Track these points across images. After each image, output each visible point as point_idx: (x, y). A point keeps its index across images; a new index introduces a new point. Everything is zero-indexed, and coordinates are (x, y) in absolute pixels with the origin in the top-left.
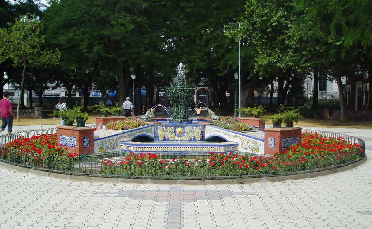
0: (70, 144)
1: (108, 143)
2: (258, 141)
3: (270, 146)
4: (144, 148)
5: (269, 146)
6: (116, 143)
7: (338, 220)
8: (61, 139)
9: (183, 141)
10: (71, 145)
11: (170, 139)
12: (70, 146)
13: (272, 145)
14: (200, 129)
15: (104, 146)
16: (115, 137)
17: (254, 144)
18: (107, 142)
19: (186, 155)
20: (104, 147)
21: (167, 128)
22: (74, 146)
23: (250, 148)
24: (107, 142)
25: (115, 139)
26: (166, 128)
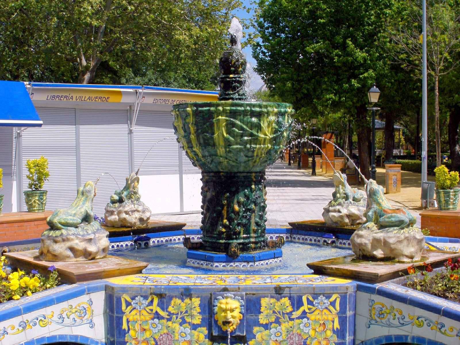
14: (333, 304)
21: (168, 304)
26: (163, 306)
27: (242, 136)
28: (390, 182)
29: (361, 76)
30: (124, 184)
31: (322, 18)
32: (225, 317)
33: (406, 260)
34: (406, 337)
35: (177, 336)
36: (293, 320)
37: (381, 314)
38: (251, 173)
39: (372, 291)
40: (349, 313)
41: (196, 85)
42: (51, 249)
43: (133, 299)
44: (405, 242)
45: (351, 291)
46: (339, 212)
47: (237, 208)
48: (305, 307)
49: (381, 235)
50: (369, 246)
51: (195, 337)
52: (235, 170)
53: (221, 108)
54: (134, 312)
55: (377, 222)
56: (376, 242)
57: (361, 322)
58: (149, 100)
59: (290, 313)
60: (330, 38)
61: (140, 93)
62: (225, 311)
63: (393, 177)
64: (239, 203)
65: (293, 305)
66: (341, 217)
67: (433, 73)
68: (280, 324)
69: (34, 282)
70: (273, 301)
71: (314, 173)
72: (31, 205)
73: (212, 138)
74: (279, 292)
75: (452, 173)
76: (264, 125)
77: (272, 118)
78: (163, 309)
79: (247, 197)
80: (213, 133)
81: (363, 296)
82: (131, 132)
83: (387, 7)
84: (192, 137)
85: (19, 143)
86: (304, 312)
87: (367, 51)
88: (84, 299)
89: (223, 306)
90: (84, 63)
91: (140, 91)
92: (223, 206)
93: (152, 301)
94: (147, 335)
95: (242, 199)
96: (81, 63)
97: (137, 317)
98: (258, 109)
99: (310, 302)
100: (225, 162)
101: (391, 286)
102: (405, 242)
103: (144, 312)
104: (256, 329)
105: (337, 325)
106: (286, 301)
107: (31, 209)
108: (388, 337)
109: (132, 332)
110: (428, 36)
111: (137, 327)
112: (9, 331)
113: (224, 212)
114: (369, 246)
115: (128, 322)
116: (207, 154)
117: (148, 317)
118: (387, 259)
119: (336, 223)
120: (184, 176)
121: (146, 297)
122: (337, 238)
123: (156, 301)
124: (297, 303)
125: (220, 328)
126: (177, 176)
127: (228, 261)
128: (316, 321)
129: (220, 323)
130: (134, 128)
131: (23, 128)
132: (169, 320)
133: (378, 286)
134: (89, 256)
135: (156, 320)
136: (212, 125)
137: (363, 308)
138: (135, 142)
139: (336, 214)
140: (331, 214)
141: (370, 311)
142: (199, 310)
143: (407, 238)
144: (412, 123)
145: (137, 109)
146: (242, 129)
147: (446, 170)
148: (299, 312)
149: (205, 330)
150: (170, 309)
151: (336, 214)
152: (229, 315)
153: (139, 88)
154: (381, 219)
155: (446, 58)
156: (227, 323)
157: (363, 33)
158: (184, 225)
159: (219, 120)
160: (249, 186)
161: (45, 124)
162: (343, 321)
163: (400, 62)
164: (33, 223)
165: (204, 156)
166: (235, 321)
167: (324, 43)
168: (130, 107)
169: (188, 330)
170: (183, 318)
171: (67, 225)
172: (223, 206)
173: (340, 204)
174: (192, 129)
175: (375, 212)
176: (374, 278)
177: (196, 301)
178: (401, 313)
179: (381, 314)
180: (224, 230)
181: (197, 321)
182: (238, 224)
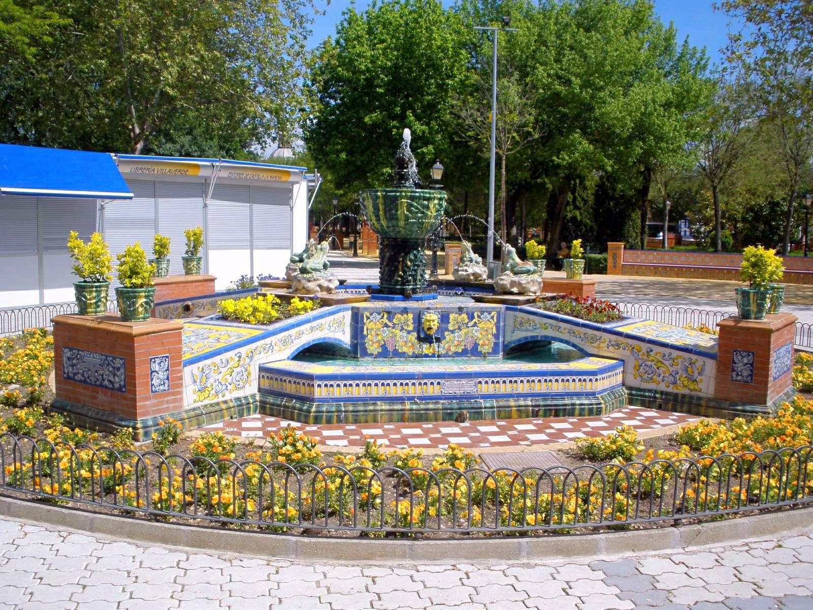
0: (103, 380)
1: (223, 370)
2: (694, 357)
3: (737, 375)
4: (281, 380)
5: (734, 376)
6: (246, 370)
7: (756, 555)
8: (69, 359)
9: (439, 356)
10: (106, 383)
11: (400, 351)
12: (101, 385)
13: (745, 374)
14: (492, 318)
15: (211, 380)
16: (244, 350)
17: (679, 366)
18: (221, 369)
19: (485, 408)
20: (212, 385)
21: (394, 318)
22: (117, 386)
23: (666, 379)
24: (221, 369)
25: (243, 355)
26: (390, 319)
27: (417, 213)
28: (450, 262)
29: (419, 151)
30: (304, 248)
31: (380, 87)
32: (430, 325)
33: (531, 294)
34: (537, 336)
35: (398, 338)
36: (468, 327)
37: (521, 324)
38: (418, 239)
39: (516, 310)
40: (502, 324)
41: (227, 153)
42: (305, 286)
43: (371, 314)
44: (531, 284)
45: (503, 310)
46: (466, 271)
47: (409, 263)
48: (476, 320)
49: (516, 278)
50: (509, 286)
51: (409, 338)
52: (409, 237)
53: (403, 194)
54: (371, 323)
55: (512, 271)
56: (513, 284)
57: (509, 330)
58: (224, 174)
59: (467, 324)
60: (386, 108)
61: (217, 166)
62: (429, 321)
63: (454, 258)
64: (411, 260)
65: (469, 318)
66: (468, 275)
67: (501, 152)
68: (461, 330)
69: (309, 304)
70: (457, 315)
71: (355, 255)
72: (190, 268)
73: (396, 214)
74: (460, 310)
75: (540, 247)
76: (431, 206)
77: (436, 202)
78: (390, 321)
79: (415, 256)
80: (397, 211)
81: (509, 312)
82: (205, 206)
83: (449, 77)
84: (381, 213)
85: (102, 214)
86: (475, 323)
87: (428, 124)
88: (340, 314)
89: (428, 318)
90: (137, 131)
91: (218, 164)
92: (399, 262)
93: (383, 316)
94: (379, 338)
95: (412, 257)
96: (133, 130)
97: (373, 326)
98: (428, 195)
99: (479, 317)
100: (403, 231)
101: (527, 307)
102: (531, 284)
103: (378, 323)
104: (446, 333)
105: (494, 331)
106: (464, 316)
107: (188, 272)
108: (526, 338)
109: (369, 337)
110: (497, 115)
111: (373, 333)
112: (305, 331)
113: (400, 267)
114: (509, 286)
115: (367, 330)
116: (390, 225)
117: (380, 326)
118: (520, 294)
119: (464, 279)
120: (255, 251)
121: (379, 314)
122: (465, 290)
123: (386, 316)
124: (471, 317)
125: (425, 333)
126: (249, 251)
127: (404, 300)
128: (482, 328)
129: (426, 329)
130: (209, 202)
131: (107, 201)
132: (393, 328)
133: (519, 307)
134: (329, 290)
135: (385, 328)
136: (397, 205)
137: (510, 322)
138: (209, 216)
139: (464, 273)
140: (460, 273)
141: (514, 322)
142: (412, 321)
143: (532, 281)
144: (459, 201)
145: (213, 182)
146: (417, 208)
147: (536, 244)
148: (472, 323)
149: (415, 334)
150: (395, 321)
151: (464, 273)
152: (432, 323)
153: (217, 161)
154: (516, 269)
155: (513, 137)
156: (430, 329)
157: (422, 103)
158: (346, 281)
159: (402, 202)
160: (416, 249)
161: (135, 197)
162: (498, 328)
163: (468, 139)
164: (194, 284)
165: (388, 227)
166: (435, 328)
167: (381, 113)
168: (205, 180)
169: (405, 334)
170: (402, 327)
171: (316, 270)
172: (399, 262)
173: (466, 265)
174: (381, 207)
175: (511, 265)
176: (517, 302)
177: (411, 316)
178: (534, 322)
179: (521, 324)
180: (400, 279)
181: (411, 328)
182: (410, 275)
